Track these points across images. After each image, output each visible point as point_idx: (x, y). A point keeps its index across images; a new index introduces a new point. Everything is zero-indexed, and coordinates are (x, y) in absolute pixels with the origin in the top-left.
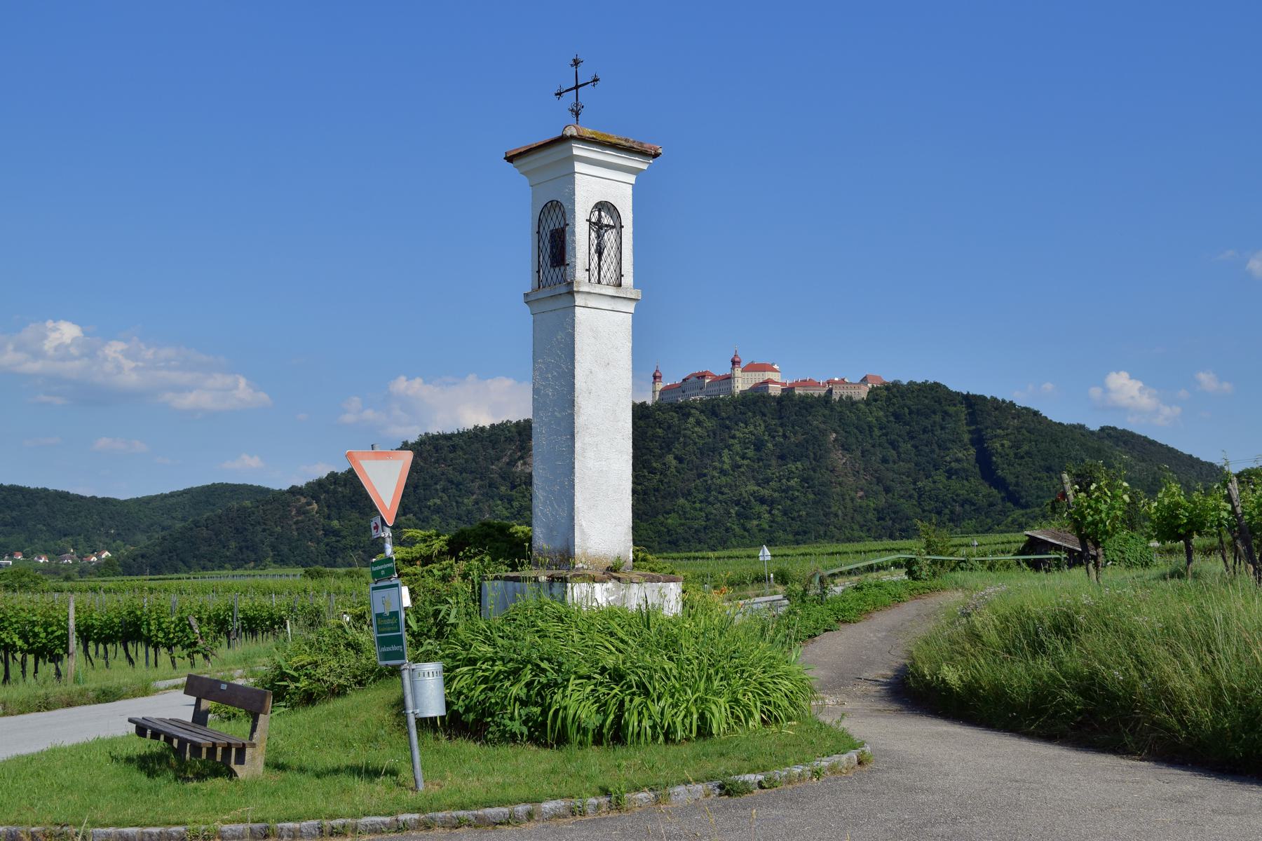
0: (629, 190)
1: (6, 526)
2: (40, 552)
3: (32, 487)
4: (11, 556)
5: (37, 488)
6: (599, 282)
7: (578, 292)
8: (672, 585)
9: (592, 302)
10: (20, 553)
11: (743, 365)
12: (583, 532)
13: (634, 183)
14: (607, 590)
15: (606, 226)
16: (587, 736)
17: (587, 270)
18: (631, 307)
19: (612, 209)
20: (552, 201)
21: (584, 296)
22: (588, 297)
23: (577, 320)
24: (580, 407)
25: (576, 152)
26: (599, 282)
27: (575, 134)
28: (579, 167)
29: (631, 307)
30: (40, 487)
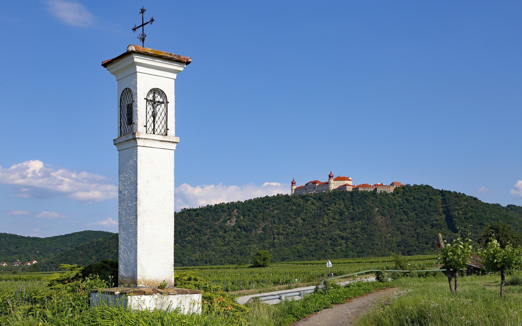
7: (139, 138)
11: (334, 177)
13: (175, 78)
15: (159, 102)
17: (145, 126)
18: (174, 146)
19: (161, 92)
20: (126, 89)
27: (134, 50)
28: (139, 69)
29: (174, 146)
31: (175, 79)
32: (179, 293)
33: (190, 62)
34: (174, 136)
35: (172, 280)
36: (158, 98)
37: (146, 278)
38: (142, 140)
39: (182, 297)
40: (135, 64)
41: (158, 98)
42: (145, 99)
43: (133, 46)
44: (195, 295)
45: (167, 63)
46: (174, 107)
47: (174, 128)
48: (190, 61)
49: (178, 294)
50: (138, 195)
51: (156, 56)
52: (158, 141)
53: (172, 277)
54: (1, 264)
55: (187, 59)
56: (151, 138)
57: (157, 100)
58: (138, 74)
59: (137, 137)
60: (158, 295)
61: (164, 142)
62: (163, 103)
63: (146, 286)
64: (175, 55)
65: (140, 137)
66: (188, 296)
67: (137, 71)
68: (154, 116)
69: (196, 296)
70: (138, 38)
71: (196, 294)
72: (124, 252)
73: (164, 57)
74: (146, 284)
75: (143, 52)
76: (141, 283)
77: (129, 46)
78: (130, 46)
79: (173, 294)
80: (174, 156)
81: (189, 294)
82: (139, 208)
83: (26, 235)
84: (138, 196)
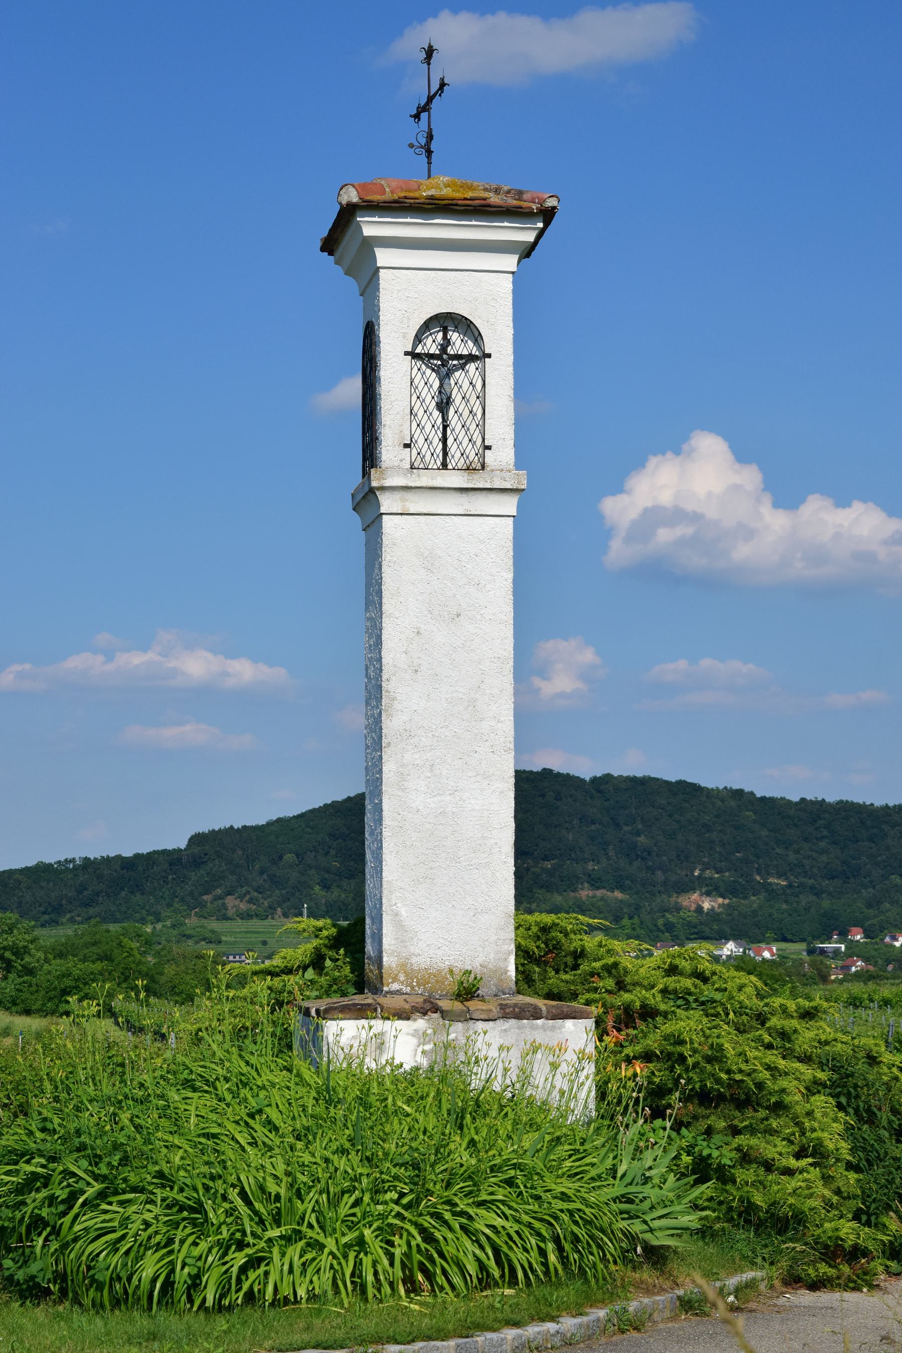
0: (507, 283)
1: (833, 878)
2: (896, 926)
3: (878, 803)
4: (843, 934)
5: (213, 831)
6: (444, 466)
7: (383, 488)
8: (569, 1024)
9: (416, 503)
10: (860, 930)
12: (400, 926)
13: (514, 269)
14: (415, 1034)
15: (458, 357)
16: (102, 1292)
18: (509, 505)
21: (397, 495)
22: (409, 495)
23: (386, 540)
24: (394, 699)
25: (368, 231)
26: (444, 466)
27: (355, 199)
28: (383, 257)
29: (509, 505)
30: (891, 804)
31: (513, 273)
32: (508, 1014)
33: (554, 208)
34: (511, 467)
35: (509, 968)
36: (460, 345)
37: (414, 960)
38: (396, 493)
39: (519, 1028)
40: (370, 244)
41: (460, 345)
42: (406, 353)
43: (351, 189)
44: (569, 1024)
45: (474, 223)
46: (511, 369)
47: (512, 442)
48: (550, 205)
49: (506, 1016)
50: (384, 677)
51: (430, 206)
52: (452, 492)
53: (506, 959)
54: (887, 939)
55: (542, 202)
56: (424, 485)
57: (434, 350)
58: (382, 272)
59: (374, 484)
60: (428, 1020)
61: (472, 493)
62: (471, 358)
63: (412, 988)
64: (508, 192)
65: (387, 483)
66: (543, 1025)
67: (379, 265)
68: (444, 405)
69: (574, 1025)
70: (411, 146)
71: (574, 1018)
72: (372, 876)
73: (458, 208)
74: (415, 984)
75: (385, 202)
76: (395, 979)
77: (341, 189)
78: (344, 190)
79: (483, 1017)
80: (511, 538)
81: (547, 1019)
82: (388, 722)
83: (260, 820)
84: (384, 684)
